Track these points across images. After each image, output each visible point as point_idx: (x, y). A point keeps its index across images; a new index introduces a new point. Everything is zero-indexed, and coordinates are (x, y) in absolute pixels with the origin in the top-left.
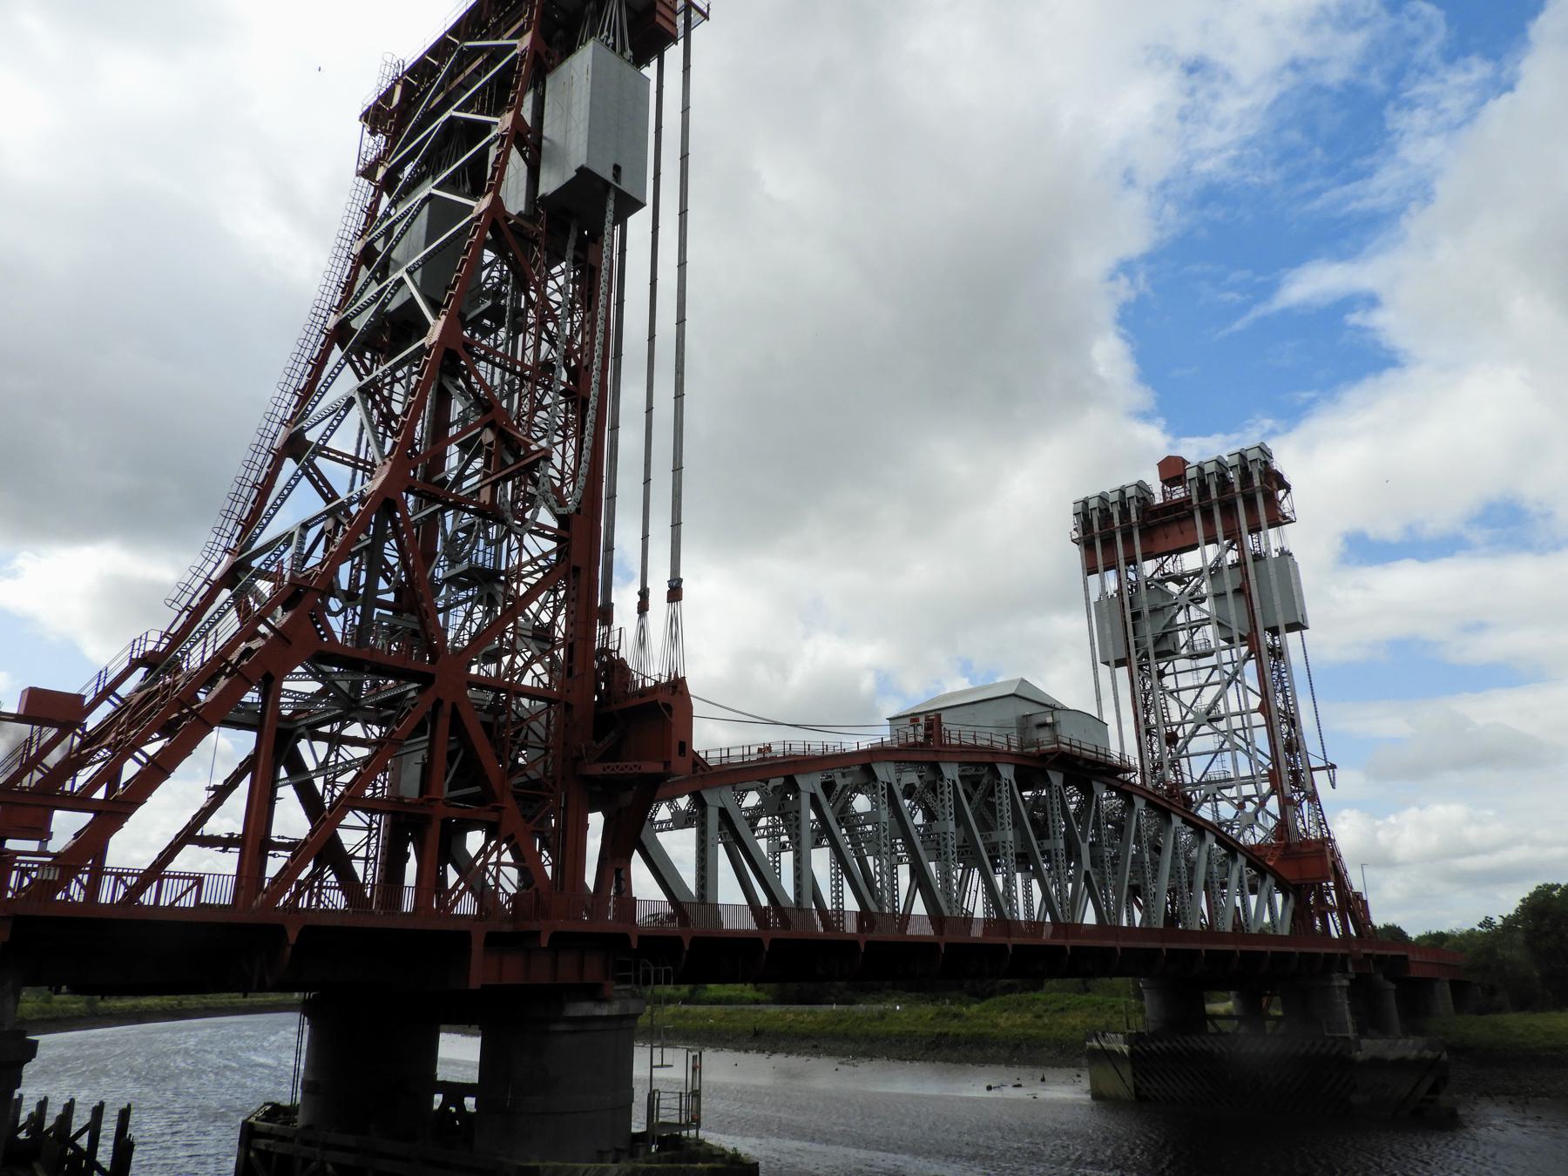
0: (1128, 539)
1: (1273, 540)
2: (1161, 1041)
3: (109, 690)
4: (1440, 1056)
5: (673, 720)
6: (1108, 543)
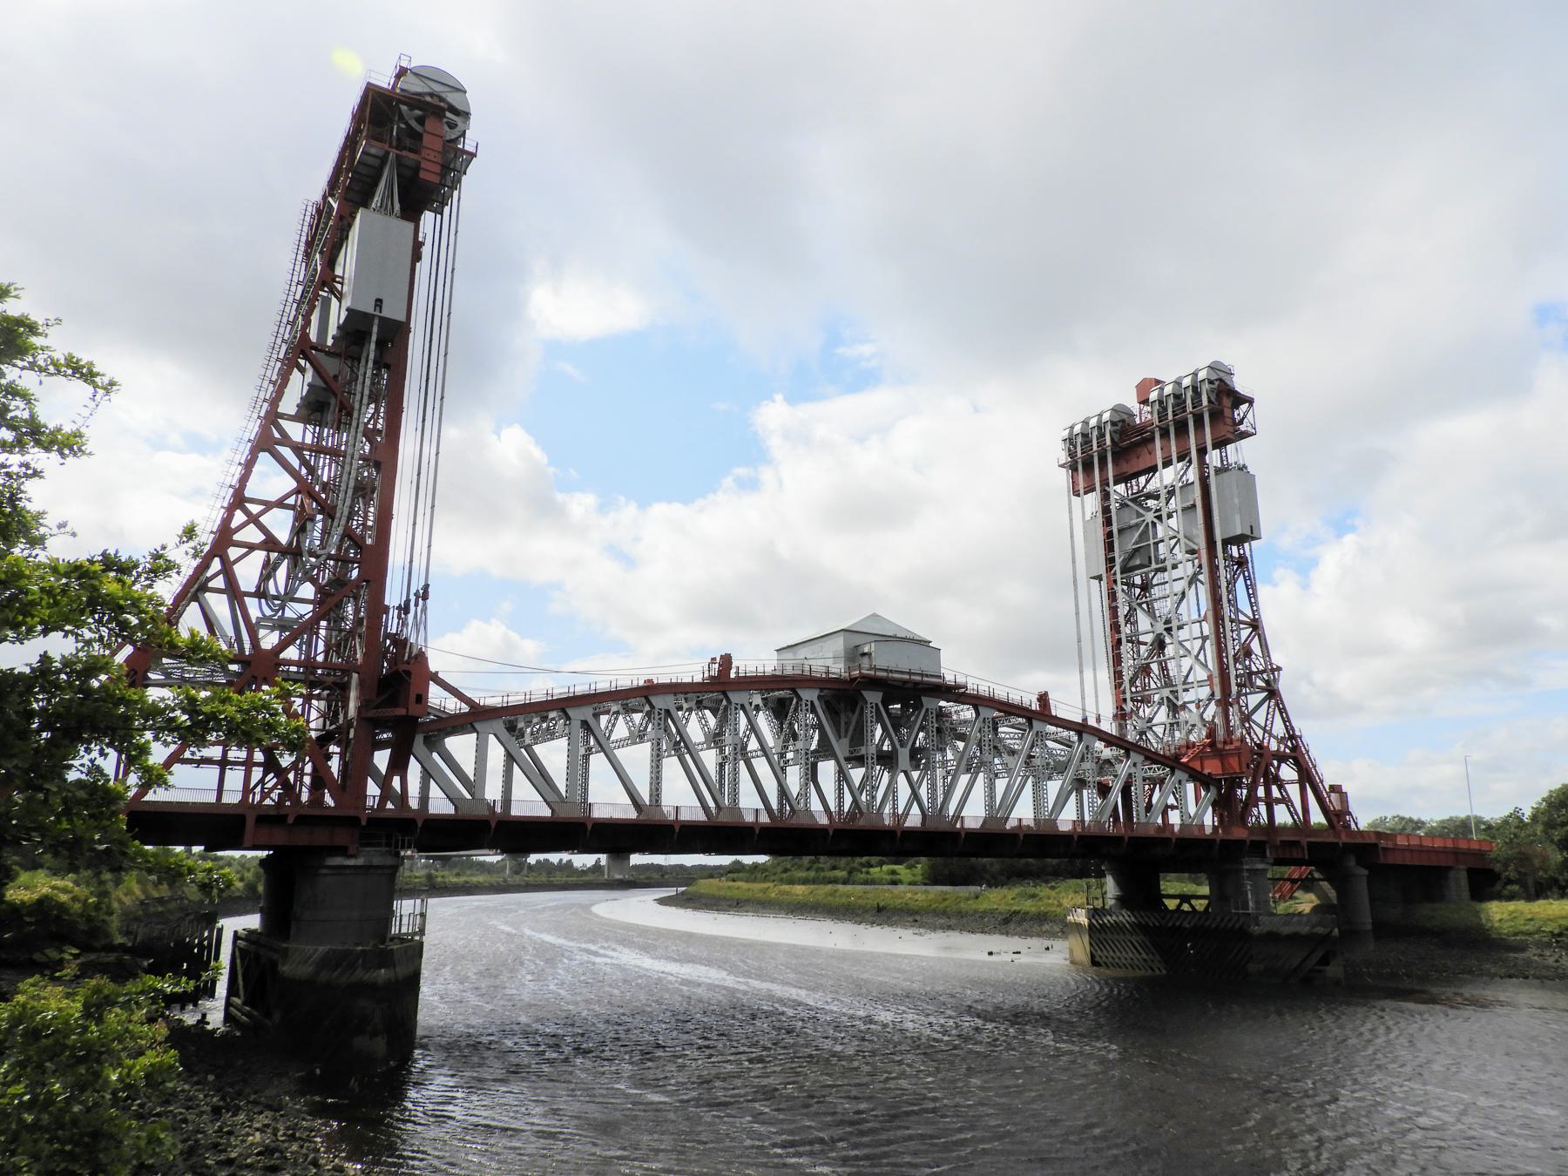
1: (1237, 452)
2: (1111, 916)
4: (1331, 932)
6: (1088, 467)
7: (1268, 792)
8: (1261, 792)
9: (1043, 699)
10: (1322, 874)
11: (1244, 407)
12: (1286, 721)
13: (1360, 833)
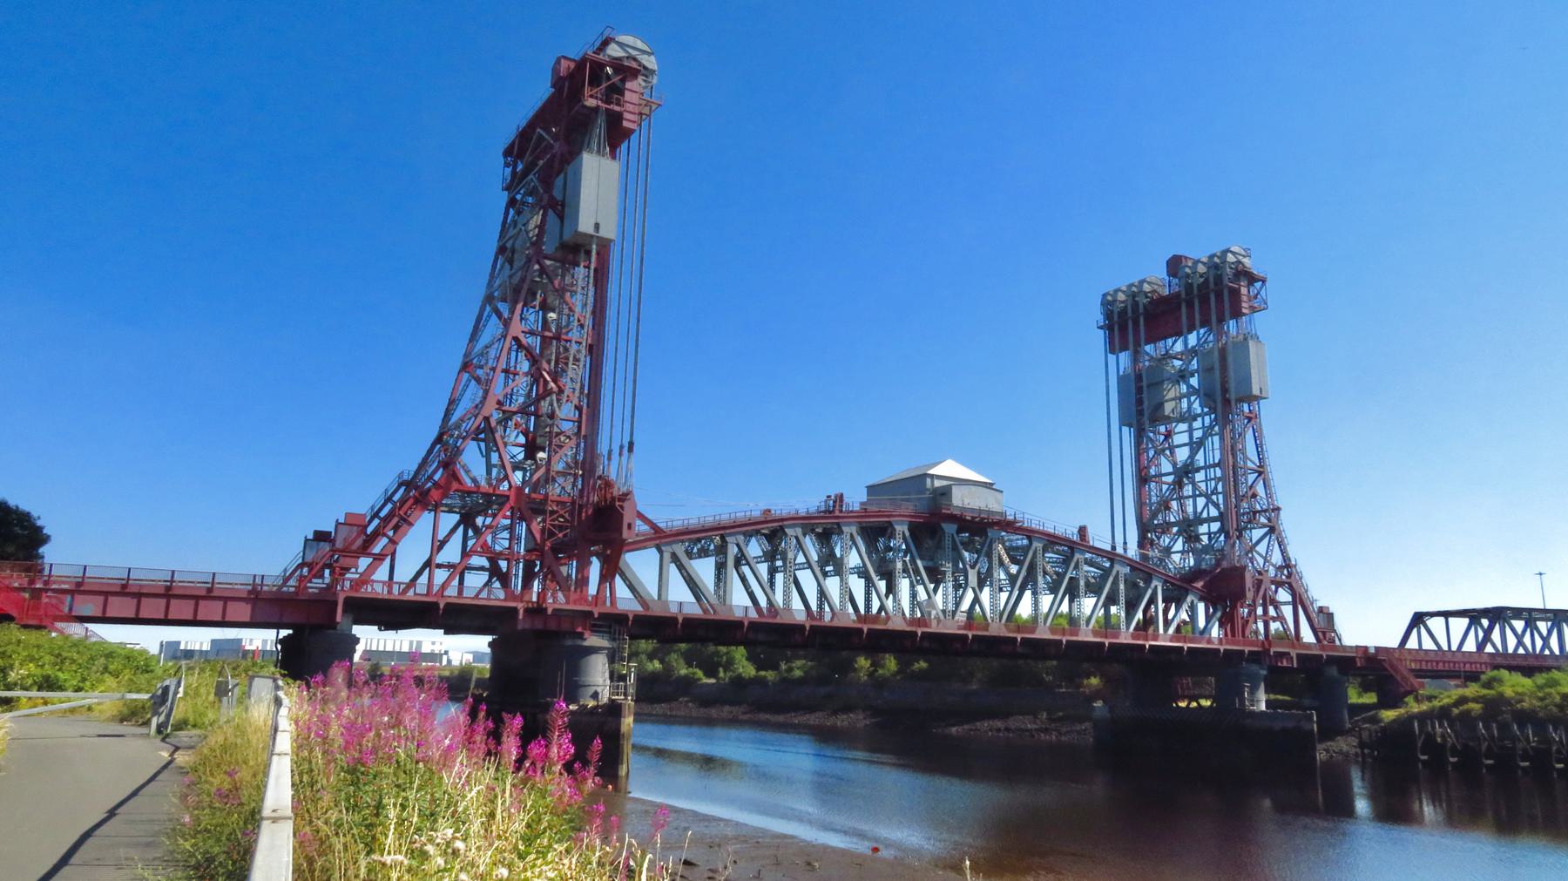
0: (1136, 324)
3: (376, 515)
5: (624, 513)
7: (1265, 612)
8: (1260, 611)
9: (1082, 531)
10: (623, 142)
11: (1258, 285)
12: (1283, 552)
13: (1344, 648)
